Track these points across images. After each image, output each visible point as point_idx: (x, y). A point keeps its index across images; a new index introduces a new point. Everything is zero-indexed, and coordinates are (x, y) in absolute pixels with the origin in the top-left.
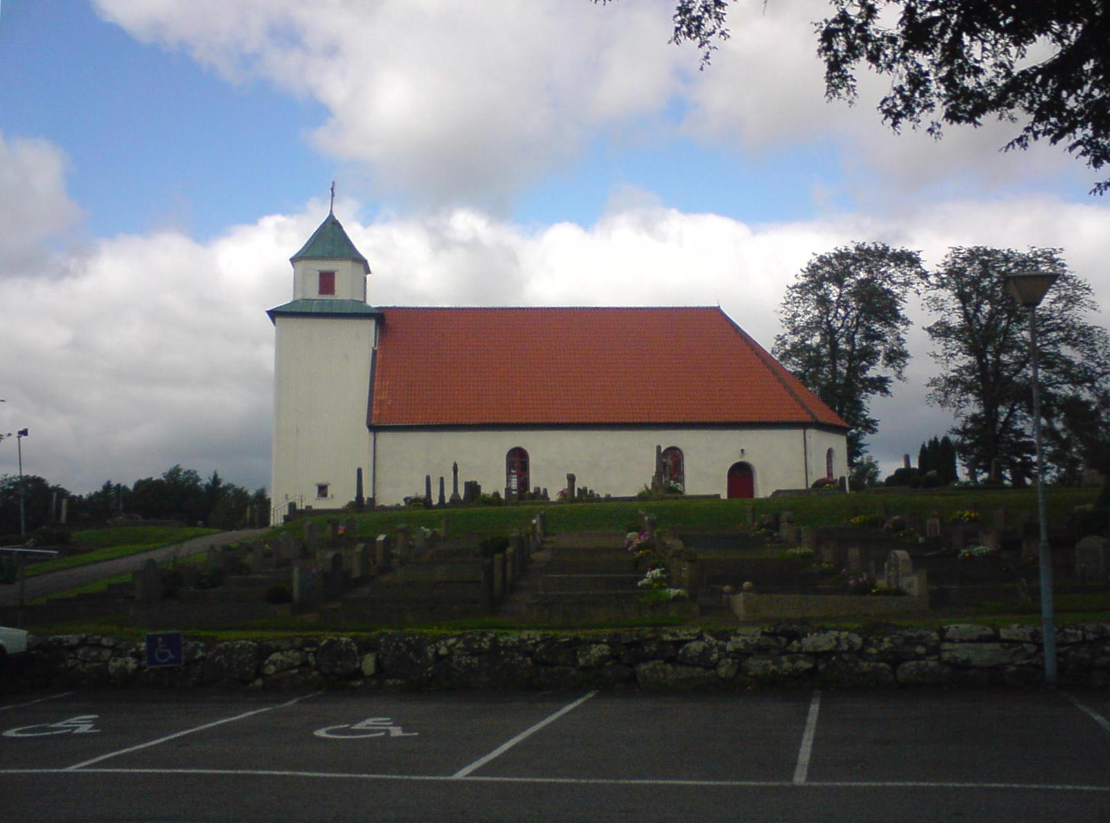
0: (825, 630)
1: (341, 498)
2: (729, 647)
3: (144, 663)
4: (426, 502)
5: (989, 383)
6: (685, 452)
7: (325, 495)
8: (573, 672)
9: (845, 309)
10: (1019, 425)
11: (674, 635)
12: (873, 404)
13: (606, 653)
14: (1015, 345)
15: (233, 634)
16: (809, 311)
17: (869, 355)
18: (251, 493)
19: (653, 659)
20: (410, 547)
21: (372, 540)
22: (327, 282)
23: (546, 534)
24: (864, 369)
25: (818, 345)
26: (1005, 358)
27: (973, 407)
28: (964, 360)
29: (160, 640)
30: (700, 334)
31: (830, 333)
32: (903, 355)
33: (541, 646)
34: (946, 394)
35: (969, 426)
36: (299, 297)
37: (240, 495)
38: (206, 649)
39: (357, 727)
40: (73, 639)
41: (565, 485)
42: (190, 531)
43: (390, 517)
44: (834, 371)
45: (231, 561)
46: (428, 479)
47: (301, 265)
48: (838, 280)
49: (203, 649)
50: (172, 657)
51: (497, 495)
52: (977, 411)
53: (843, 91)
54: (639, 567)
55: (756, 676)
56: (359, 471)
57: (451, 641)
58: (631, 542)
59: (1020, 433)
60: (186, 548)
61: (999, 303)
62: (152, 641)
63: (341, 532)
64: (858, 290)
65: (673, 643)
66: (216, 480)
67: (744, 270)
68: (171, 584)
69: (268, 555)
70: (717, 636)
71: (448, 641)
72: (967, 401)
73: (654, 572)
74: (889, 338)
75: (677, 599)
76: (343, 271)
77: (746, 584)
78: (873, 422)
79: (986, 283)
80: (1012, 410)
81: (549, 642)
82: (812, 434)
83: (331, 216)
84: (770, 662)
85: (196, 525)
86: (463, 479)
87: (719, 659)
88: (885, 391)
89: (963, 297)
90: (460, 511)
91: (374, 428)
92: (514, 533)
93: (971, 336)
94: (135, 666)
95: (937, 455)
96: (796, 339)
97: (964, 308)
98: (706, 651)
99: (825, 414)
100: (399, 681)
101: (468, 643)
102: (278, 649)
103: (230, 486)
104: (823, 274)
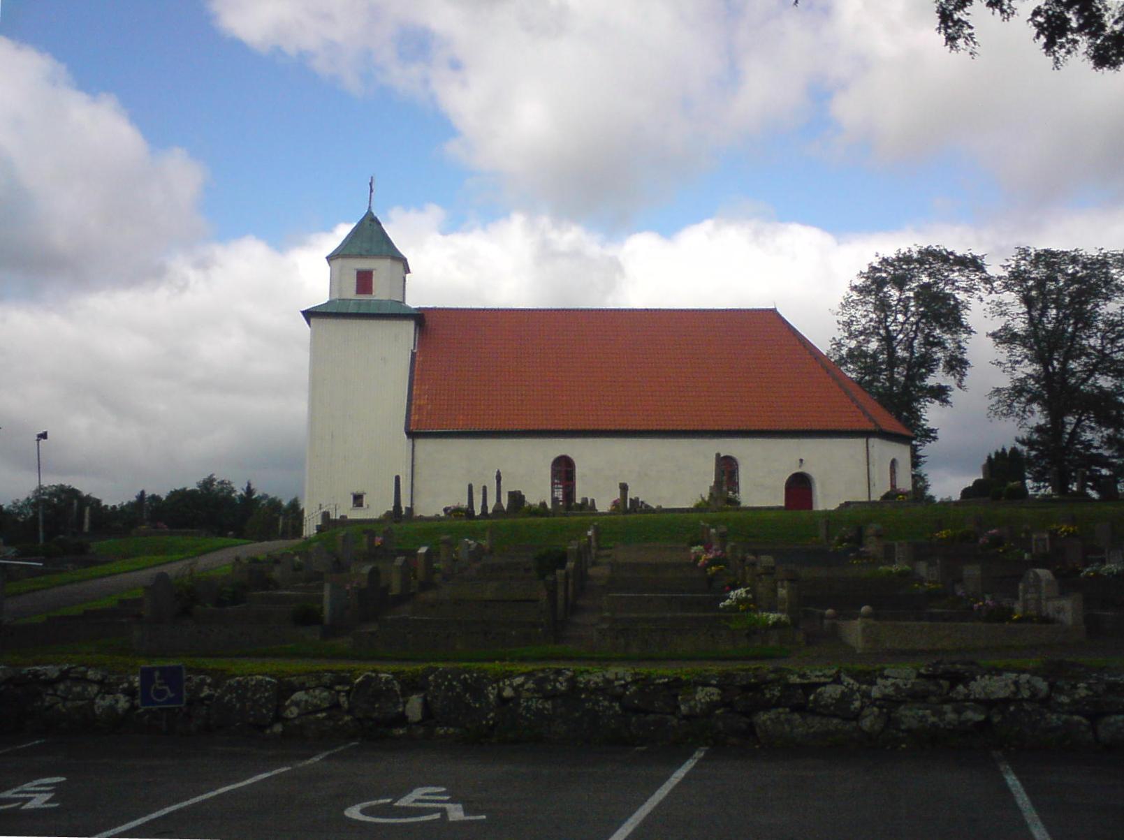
0: (999, 672)
1: (378, 507)
2: (875, 692)
3: (138, 702)
4: (469, 512)
5: (1055, 392)
6: (740, 461)
7: (361, 505)
8: (674, 721)
9: (905, 314)
10: (1088, 435)
11: (803, 676)
12: (931, 413)
13: (715, 698)
14: (1083, 351)
15: (247, 665)
16: (864, 315)
17: (927, 363)
18: (285, 503)
19: (777, 706)
20: (455, 561)
21: (412, 554)
22: (364, 281)
23: (600, 548)
24: (922, 377)
25: (875, 352)
26: (1073, 365)
27: (1038, 417)
28: (1028, 368)
29: (157, 674)
30: (757, 335)
31: (888, 339)
32: (964, 363)
33: (633, 689)
34: (1010, 406)
35: (1035, 436)
36: (336, 296)
37: (275, 505)
38: (214, 686)
39: (405, 801)
40: (52, 671)
41: (617, 495)
42: (221, 541)
43: (431, 528)
44: (891, 379)
45: (256, 577)
46: (470, 487)
47: (339, 262)
48: (900, 282)
49: (209, 685)
50: (171, 695)
51: (543, 505)
52: (1042, 422)
53: (960, 42)
54: (715, 586)
55: (909, 731)
56: (397, 478)
57: (518, 680)
58: (697, 559)
59: (1088, 445)
60: (203, 562)
61: (1067, 307)
62: (147, 675)
63: (378, 543)
64: (920, 295)
65: (802, 686)
66: (249, 491)
67: (802, 275)
68: (185, 602)
69: (298, 568)
70: (857, 676)
71: (515, 679)
72: (1032, 412)
73: (739, 591)
74: (950, 345)
75: (777, 625)
76: (381, 269)
77: (865, 609)
78: (932, 431)
79: (1051, 286)
80: (1079, 421)
81: (643, 682)
82: (875, 442)
83: (370, 213)
84: (928, 712)
85: (226, 536)
86: (506, 488)
87: (862, 708)
88: (945, 401)
89: (1027, 301)
90: (487, 522)
91: (412, 435)
92: (572, 547)
93: (1037, 342)
94: (127, 705)
95: (1002, 470)
96: (853, 344)
97: (1029, 312)
98: (846, 698)
99: (889, 422)
100: (451, 730)
101: (540, 682)
102: (302, 687)
103: (265, 496)
104: (875, 283)
